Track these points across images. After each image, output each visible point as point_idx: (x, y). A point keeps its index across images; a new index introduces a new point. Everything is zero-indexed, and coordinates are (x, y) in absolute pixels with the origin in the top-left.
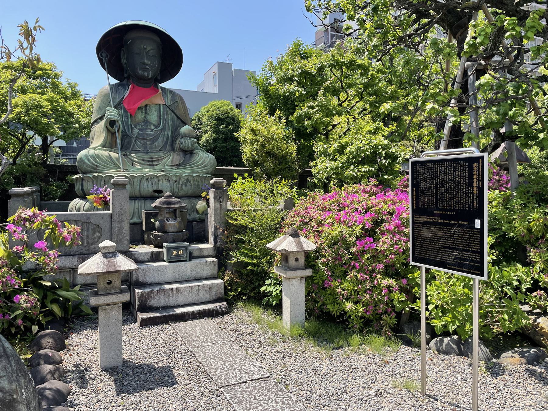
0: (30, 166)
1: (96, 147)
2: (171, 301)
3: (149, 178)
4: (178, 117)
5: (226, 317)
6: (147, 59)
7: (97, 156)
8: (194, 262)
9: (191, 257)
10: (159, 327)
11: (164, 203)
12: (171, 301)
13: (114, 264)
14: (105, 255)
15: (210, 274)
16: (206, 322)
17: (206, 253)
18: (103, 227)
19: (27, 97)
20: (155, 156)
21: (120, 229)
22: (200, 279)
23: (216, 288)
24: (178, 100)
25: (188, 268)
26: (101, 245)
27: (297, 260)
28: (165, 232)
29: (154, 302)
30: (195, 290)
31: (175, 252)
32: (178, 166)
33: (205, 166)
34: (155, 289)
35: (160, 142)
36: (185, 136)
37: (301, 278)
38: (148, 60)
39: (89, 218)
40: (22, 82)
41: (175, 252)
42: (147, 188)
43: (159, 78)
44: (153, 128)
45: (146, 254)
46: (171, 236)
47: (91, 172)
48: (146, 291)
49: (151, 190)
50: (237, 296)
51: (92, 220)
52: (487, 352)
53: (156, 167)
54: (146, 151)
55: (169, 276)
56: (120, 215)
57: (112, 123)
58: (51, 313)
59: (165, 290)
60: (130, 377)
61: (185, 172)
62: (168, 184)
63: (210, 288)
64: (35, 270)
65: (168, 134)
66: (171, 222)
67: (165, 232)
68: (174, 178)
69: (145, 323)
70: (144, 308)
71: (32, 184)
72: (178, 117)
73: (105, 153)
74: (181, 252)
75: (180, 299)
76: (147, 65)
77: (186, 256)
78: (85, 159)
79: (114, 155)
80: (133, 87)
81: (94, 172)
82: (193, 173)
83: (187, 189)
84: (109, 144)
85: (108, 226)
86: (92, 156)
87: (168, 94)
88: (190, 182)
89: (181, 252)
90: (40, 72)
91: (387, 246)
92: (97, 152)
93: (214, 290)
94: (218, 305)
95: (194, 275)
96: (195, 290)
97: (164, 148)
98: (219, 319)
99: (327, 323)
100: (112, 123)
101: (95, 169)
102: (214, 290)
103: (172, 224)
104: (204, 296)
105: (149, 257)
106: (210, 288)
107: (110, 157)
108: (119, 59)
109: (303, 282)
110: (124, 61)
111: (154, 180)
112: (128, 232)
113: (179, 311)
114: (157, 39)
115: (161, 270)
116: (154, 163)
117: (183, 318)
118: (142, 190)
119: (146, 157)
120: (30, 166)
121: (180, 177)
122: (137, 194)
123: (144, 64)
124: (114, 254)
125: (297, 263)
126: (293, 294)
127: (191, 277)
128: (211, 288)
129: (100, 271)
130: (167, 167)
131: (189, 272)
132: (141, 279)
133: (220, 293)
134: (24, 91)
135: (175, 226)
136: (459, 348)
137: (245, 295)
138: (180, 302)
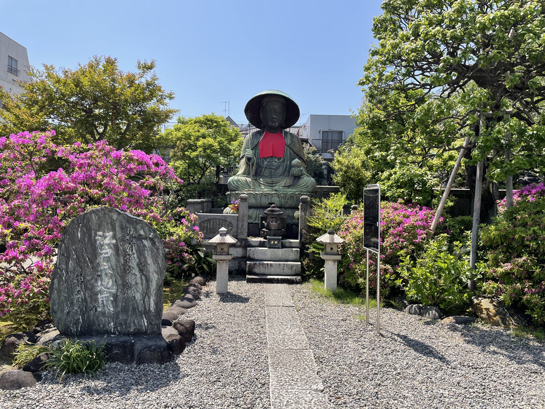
0: (208, 185)
1: (239, 176)
2: (266, 271)
3: (266, 195)
4: (294, 152)
5: (299, 286)
6: (275, 115)
7: (239, 180)
8: (284, 249)
9: (283, 246)
10: (256, 284)
11: (270, 211)
12: (267, 271)
13: (224, 239)
14: (221, 235)
15: (294, 258)
16: (285, 285)
17: (294, 245)
18: (233, 224)
19: (205, 141)
20: (274, 179)
21: (242, 225)
22: (287, 261)
23: (296, 267)
24: (295, 140)
25: (280, 252)
26: (220, 230)
27: (332, 249)
28: (270, 230)
29: (256, 270)
30: (281, 266)
31: (273, 242)
32: (289, 187)
33: (307, 187)
34: (258, 263)
35: (281, 170)
36: (295, 166)
37: (334, 261)
38: (275, 115)
39: (226, 218)
40: (203, 130)
41: (273, 242)
42: (265, 201)
43: (284, 126)
44: (276, 160)
45: (256, 242)
46: (272, 232)
47: (235, 191)
48: (252, 263)
49: (267, 202)
50: (310, 275)
51: (228, 219)
52: (435, 314)
53: (274, 188)
54: (271, 176)
55: (268, 256)
56: (243, 217)
57: (249, 159)
58: (202, 268)
59: (263, 264)
60: (226, 297)
61: (290, 191)
62: (278, 199)
63: (292, 267)
64: (196, 245)
65: (287, 165)
66: (274, 223)
67: (270, 230)
68: (282, 195)
69: (250, 281)
70: (251, 273)
71: (208, 197)
72: (294, 152)
73: (244, 178)
74: (276, 242)
75: (272, 271)
76: (275, 118)
77: (280, 245)
78: (231, 182)
79: (249, 180)
80: (266, 134)
81: (235, 191)
82: (296, 192)
83: (290, 203)
84: (247, 173)
85: (236, 223)
86: (236, 181)
87: (289, 136)
88: (293, 198)
89: (276, 242)
90: (215, 124)
91: (388, 244)
92: (239, 178)
93: (294, 268)
94: (294, 277)
95: (284, 257)
96: (281, 266)
97: (283, 174)
98: (294, 286)
99: (348, 289)
100: (249, 159)
101: (237, 189)
102: (294, 268)
103: (274, 225)
104: (287, 271)
105: (258, 244)
106: (292, 267)
107: (246, 181)
108: (259, 116)
109: (336, 263)
110: (261, 116)
111: (269, 196)
112: (247, 228)
113: (269, 277)
114: (283, 101)
115: (264, 253)
116: (274, 185)
117: (271, 281)
118: (262, 202)
119: (269, 180)
120: (208, 185)
121: (286, 195)
122: (259, 205)
123: (272, 118)
124: (225, 235)
125: (332, 251)
126: (330, 269)
127: (277, 257)
128: (292, 266)
129: (240, 256)
130: (281, 188)
131: (280, 256)
132: (251, 256)
133: (298, 271)
134: (204, 137)
135: (275, 226)
136: (420, 311)
137: (316, 274)
138: (272, 273)
